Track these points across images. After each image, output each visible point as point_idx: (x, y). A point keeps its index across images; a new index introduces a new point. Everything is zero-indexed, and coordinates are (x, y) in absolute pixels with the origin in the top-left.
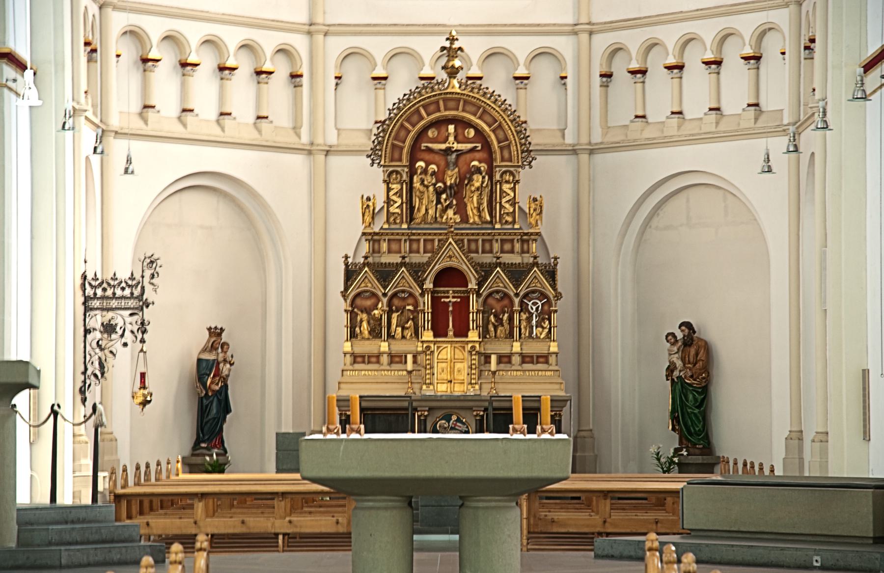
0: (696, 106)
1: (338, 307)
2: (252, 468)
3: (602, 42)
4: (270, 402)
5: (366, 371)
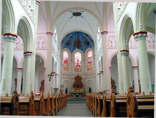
2: (68, 94)
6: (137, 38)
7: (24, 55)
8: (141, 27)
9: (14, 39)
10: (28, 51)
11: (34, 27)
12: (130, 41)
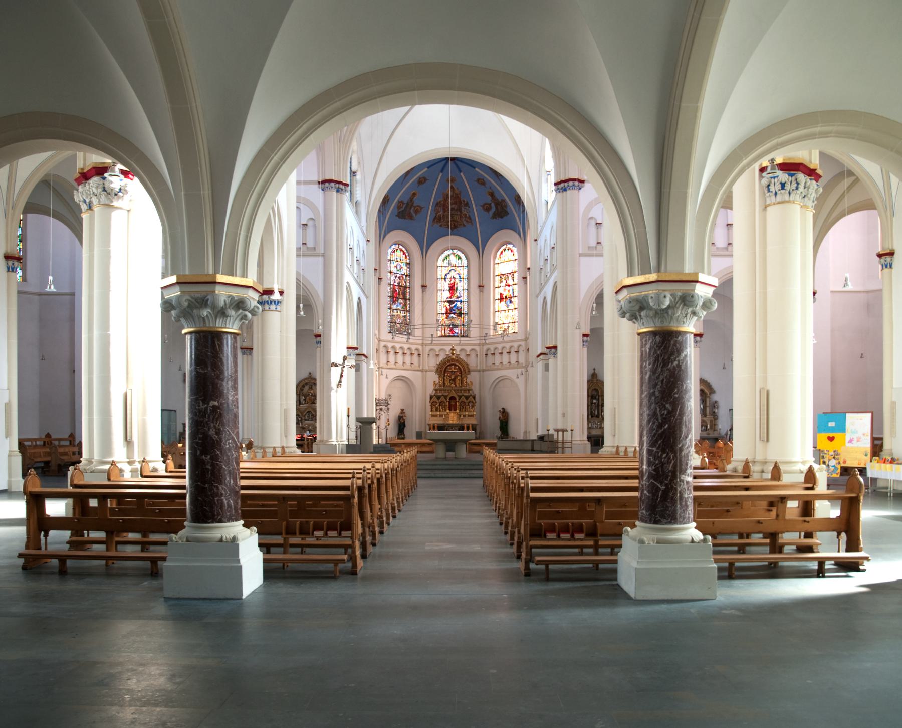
0: (505, 362)
1: (429, 405)
3: (485, 348)
4: (414, 426)
5: (435, 418)
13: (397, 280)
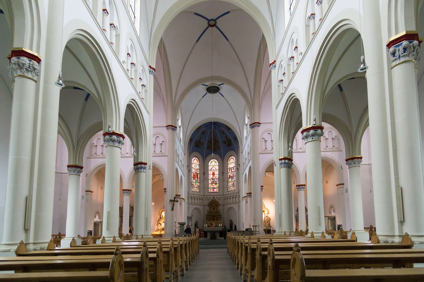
1: (206, 218)
3: (225, 196)
6: (306, 137)
7: (134, 168)
8: (314, 122)
9: (120, 142)
10: (140, 161)
11: (149, 118)
12: (295, 139)
13: (195, 171)
